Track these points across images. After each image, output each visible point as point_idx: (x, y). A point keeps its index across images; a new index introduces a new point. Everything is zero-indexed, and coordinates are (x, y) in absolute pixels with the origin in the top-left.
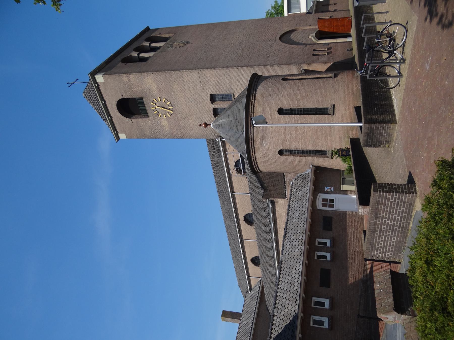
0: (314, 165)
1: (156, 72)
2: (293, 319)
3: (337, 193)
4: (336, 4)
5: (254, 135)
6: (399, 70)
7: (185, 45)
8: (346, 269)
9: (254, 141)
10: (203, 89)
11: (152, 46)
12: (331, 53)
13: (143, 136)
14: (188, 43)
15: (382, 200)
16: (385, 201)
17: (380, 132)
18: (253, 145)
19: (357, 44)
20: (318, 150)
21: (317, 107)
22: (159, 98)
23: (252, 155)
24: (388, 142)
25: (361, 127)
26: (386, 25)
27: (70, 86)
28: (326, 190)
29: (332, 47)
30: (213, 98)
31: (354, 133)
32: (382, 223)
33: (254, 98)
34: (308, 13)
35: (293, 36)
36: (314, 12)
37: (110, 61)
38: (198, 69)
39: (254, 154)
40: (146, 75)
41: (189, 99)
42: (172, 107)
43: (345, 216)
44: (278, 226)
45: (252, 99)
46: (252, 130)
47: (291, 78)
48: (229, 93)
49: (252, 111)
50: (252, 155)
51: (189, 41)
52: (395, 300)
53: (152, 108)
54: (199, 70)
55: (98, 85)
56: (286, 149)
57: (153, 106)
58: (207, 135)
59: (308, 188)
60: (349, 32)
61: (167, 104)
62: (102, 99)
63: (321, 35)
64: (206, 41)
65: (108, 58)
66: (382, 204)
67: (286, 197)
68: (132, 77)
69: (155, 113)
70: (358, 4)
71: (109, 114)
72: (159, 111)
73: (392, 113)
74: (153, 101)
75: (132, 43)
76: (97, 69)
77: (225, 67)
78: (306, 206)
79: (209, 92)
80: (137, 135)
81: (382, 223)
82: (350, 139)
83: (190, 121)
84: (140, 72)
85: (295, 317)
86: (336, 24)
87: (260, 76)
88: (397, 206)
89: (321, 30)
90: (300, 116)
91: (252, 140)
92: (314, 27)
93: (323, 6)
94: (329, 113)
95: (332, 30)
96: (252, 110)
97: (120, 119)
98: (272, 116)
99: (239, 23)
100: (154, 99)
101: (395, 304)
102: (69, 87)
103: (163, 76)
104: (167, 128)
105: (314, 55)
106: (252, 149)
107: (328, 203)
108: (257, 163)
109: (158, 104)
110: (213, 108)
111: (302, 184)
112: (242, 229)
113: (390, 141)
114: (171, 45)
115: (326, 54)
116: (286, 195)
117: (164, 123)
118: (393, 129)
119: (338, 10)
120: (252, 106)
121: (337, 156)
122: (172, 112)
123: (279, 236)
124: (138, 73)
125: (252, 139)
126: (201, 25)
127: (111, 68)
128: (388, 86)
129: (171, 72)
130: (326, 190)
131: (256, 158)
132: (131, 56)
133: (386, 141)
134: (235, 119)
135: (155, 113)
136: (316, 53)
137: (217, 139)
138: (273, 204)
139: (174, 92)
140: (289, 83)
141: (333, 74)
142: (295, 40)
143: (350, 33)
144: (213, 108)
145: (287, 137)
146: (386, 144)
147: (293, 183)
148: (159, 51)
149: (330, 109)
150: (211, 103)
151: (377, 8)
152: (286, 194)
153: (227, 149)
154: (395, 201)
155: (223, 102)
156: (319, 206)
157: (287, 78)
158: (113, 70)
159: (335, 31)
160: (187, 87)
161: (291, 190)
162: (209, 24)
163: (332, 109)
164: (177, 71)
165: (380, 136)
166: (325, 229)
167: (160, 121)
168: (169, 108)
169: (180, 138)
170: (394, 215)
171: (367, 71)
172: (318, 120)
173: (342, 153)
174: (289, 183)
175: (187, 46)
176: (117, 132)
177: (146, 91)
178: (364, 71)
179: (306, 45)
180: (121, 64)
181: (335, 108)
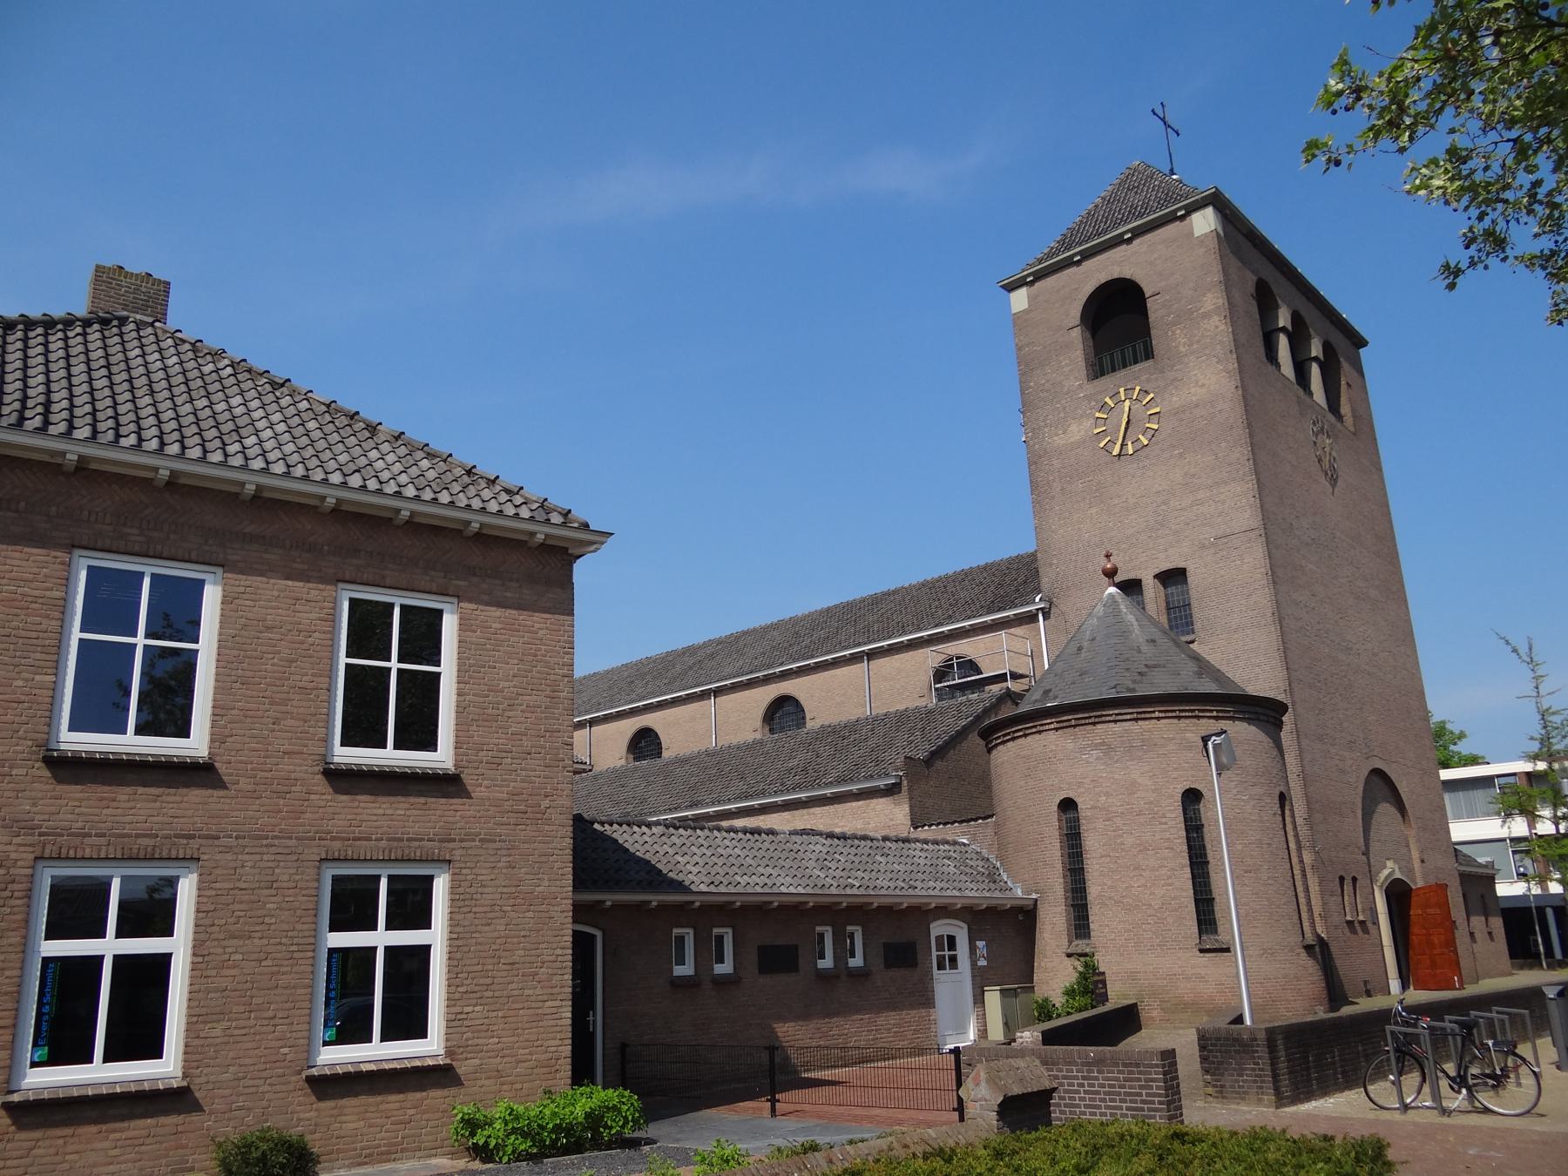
0: (1039, 906)
1: (1244, 397)
2: (672, 881)
3: (974, 976)
4: (1492, 940)
5: (1112, 725)
6: (1413, 1108)
7: (1327, 474)
8: (805, 1016)
9: (1094, 724)
10: (1203, 547)
11: (1311, 367)
12: (1354, 931)
13: (1027, 366)
14: (1333, 481)
15: (1139, 1073)
16: (1139, 1080)
17: (1246, 1069)
18: (1083, 722)
19: (1432, 1003)
20: (1090, 913)
21: (1217, 900)
22: (1157, 410)
23: (1049, 721)
24: (1221, 1092)
25: (1239, 1020)
26: (1533, 1062)
27: (1155, 114)
28: (977, 943)
29: (1368, 933)
30: (1173, 577)
31: (1155, 1014)
32: (1076, 1078)
33: (1220, 715)
34: (1456, 851)
35: (1385, 811)
36: (1463, 868)
37: (1255, 246)
38: (1265, 529)
39: (1052, 726)
40: (1231, 368)
41: (1164, 503)
42: (1131, 452)
43: (924, 1004)
44: (817, 810)
45: (1218, 711)
46: (1128, 717)
47: (1288, 819)
48: (1197, 626)
49: (1184, 714)
50: (1049, 721)
51: (1339, 483)
52: (1018, 1096)
53: (1122, 390)
54: (1262, 532)
55: (1182, 218)
56: (1082, 821)
57: (1131, 392)
58: (1051, 565)
59: (975, 892)
60: (1414, 986)
61: (1140, 436)
62: (1138, 233)
63: (1399, 895)
64: (1344, 538)
65: (1280, 250)
66: (1130, 1073)
67: (915, 828)
68: (1218, 323)
69: (1107, 400)
70: (1552, 996)
71: (1087, 255)
72: (1114, 412)
73: (1296, 1099)
74: (1147, 392)
75: (1313, 303)
76: (1231, 210)
77: (1278, 611)
78: (930, 890)
79: (1195, 566)
80: (1027, 345)
81: (1076, 1078)
82: (1135, 1005)
83: (1094, 510)
84: (1237, 347)
85: (679, 886)
86: (1436, 941)
87: (1279, 725)
88: (1128, 1109)
89: (1413, 895)
90: (1186, 855)
91: (1097, 720)
92: (1418, 874)
93: (1482, 896)
94: (1204, 937)
95: (1416, 930)
96: (1187, 714)
97: (1076, 289)
98: (1175, 774)
99: (1405, 636)
100: (1152, 395)
101: (1013, 1097)
102: (1153, 111)
103: (1231, 421)
104: (1059, 441)
105: (1342, 879)
106: (1070, 720)
107: (947, 953)
108: (1025, 735)
109: (1137, 406)
110: (1140, 580)
111: (975, 873)
112: (747, 693)
113: (1223, 1098)
114: (1322, 429)
115: (1349, 918)
116: (923, 827)
117: (1078, 431)
118: (1260, 1100)
119: (1474, 945)
120: (1199, 710)
121: (1081, 969)
122: (1114, 453)
123: (786, 815)
124: (1234, 340)
125: (1100, 719)
126: (1389, 513)
127: (1237, 252)
128: (1373, 1081)
129: (1246, 443)
130: (977, 943)
131: (1040, 732)
132: (1277, 307)
133: (1222, 1086)
134: (1149, 663)
135: (1107, 400)
136: (1348, 887)
137: (1040, 596)
138: (891, 791)
139: (1181, 455)
140: (1275, 814)
141: (1312, 943)
142: (1376, 818)
143: (1412, 988)
144: (1140, 580)
145: (1118, 821)
146: (1214, 1086)
147: (964, 845)
148: (1301, 392)
149: (1217, 941)
150: (1157, 571)
151: (1546, 1049)
152: (926, 828)
153: (1012, 630)
154: (1143, 1102)
155: (1164, 611)
156: (939, 928)
157: (1287, 807)
158: (1234, 261)
159: (1414, 939)
160: (1201, 495)
161: (947, 842)
162: (1393, 538)
163: (1217, 946)
164: (1251, 462)
165: (1234, 1069)
166: (887, 947)
167: (1082, 416)
168: (1129, 443)
169: (1031, 482)
170: (1103, 1104)
171: (1407, 1024)
172: (1180, 907)
173: (1091, 984)
174: (964, 834)
175: (1323, 480)
176: (1032, 283)
177: (1178, 367)
178: (1403, 1017)
179: (1366, 853)
180: (1251, 279)
181: (1220, 954)
